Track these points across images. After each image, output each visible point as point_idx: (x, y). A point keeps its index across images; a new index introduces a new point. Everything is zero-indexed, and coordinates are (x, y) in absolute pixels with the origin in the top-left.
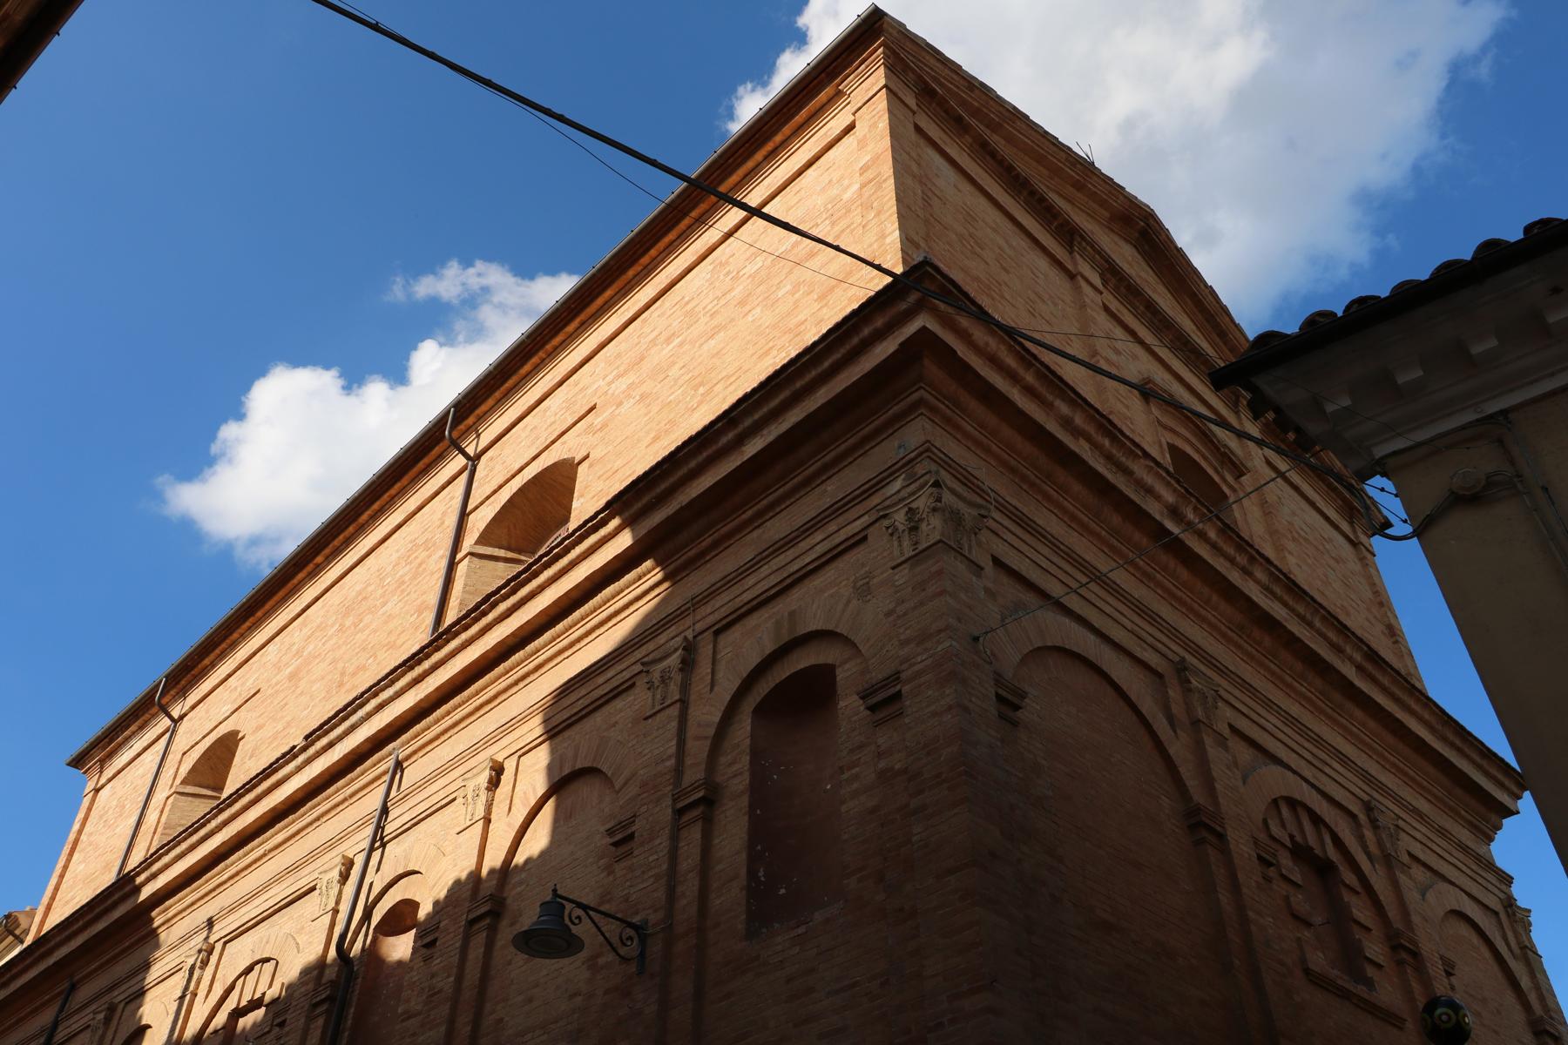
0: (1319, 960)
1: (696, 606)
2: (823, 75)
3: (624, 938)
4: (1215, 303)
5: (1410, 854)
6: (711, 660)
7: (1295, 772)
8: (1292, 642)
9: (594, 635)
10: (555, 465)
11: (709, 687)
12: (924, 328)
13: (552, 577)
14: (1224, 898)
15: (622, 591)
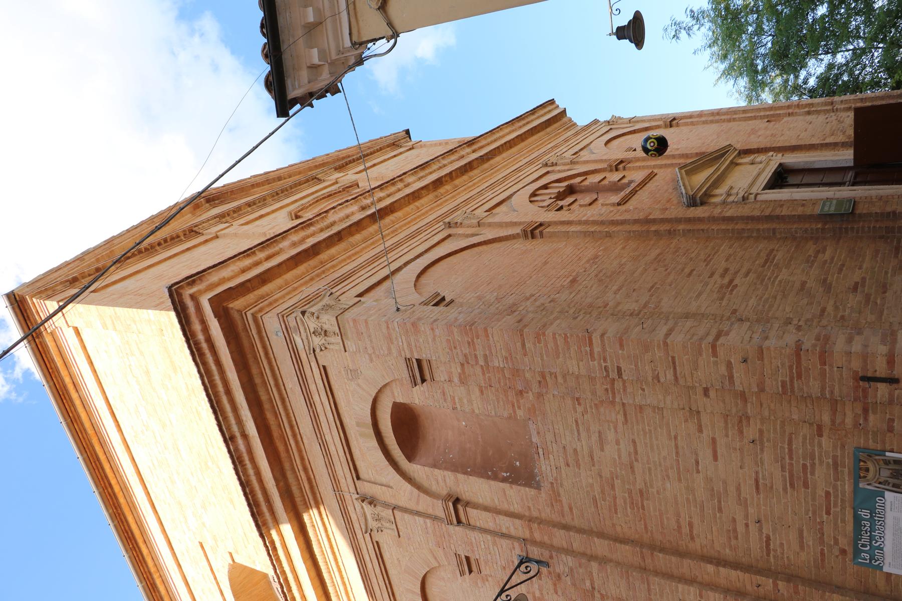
0: (615, 198)
1: (339, 489)
2: (37, 340)
3: (525, 571)
4: (261, 177)
5: (574, 155)
6: (374, 485)
7: (518, 190)
8: (451, 176)
9: (342, 567)
10: (230, 580)
11: (390, 489)
12: (209, 300)
13: (298, 587)
14: (573, 228)
15: (318, 540)
